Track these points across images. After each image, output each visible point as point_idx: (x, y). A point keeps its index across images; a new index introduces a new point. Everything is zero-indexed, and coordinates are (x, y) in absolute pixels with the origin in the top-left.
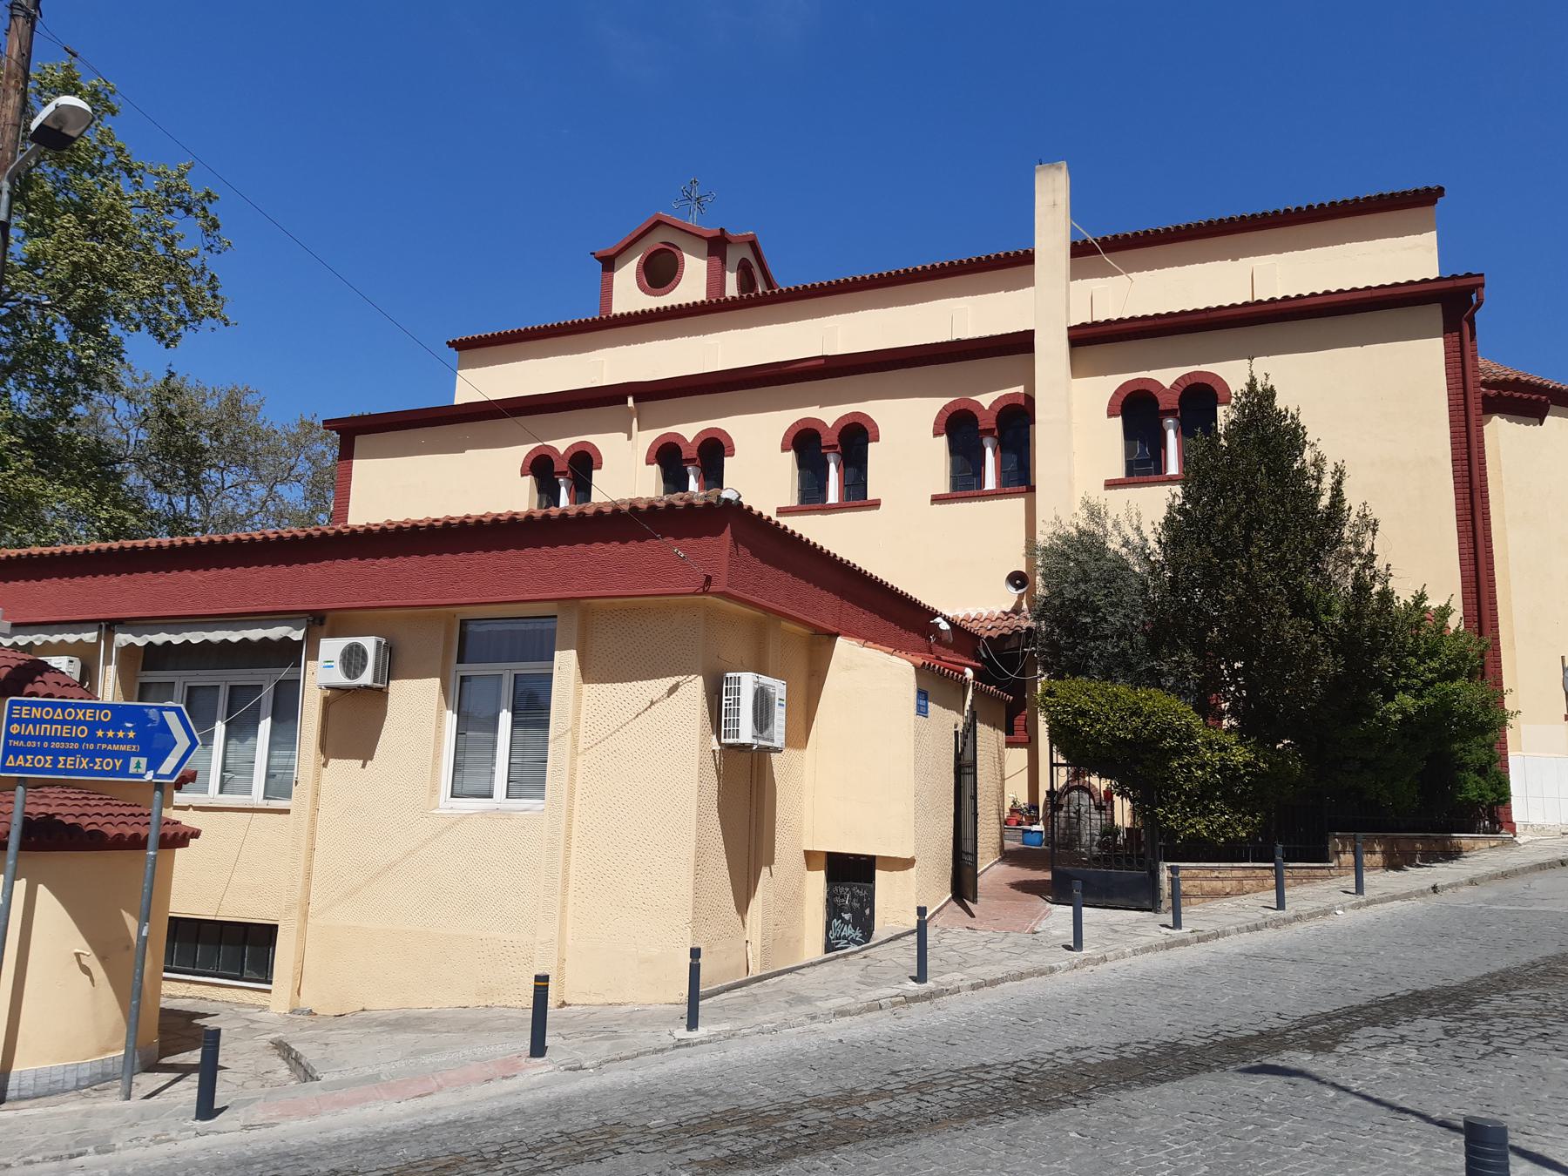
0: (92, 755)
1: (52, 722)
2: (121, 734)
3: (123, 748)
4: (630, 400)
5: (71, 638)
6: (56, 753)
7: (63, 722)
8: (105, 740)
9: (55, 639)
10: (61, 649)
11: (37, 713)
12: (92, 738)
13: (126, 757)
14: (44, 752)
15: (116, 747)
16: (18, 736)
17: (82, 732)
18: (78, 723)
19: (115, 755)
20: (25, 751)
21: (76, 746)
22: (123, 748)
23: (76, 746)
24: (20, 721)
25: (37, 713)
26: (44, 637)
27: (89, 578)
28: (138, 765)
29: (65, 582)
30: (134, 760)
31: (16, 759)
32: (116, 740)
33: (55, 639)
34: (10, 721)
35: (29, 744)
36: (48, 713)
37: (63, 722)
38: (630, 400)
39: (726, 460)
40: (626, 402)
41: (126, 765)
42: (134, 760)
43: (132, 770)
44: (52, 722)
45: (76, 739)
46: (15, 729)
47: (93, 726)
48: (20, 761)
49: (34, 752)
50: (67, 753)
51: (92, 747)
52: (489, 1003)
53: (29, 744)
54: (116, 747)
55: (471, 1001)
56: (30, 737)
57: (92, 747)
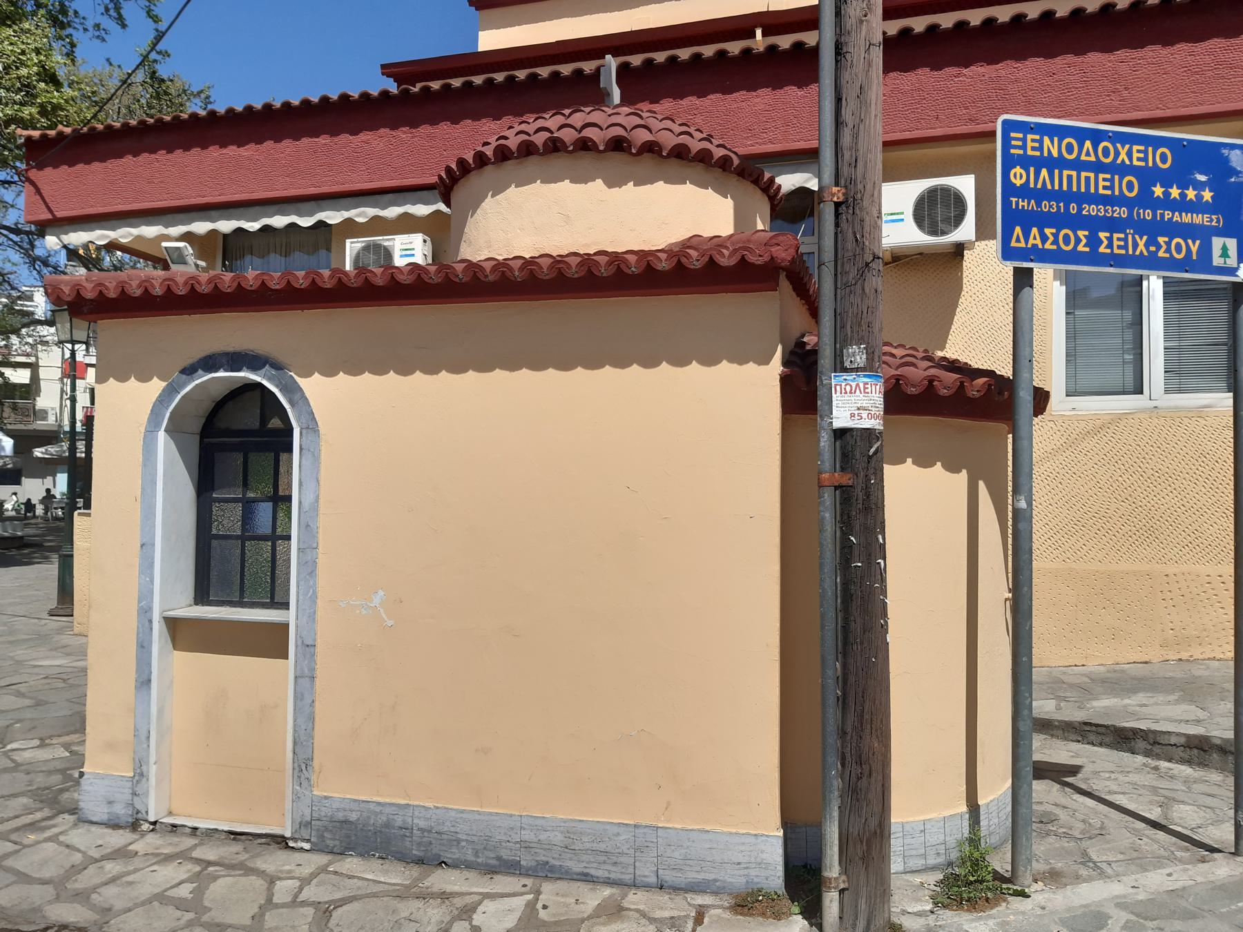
0: (1152, 230)
1: (1078, 165)
2: (1191, 194)
3: (1198, 219)
4: (759, 32)
5: (422, 210)
6: (1094, 225)
7: (1098, 167)
8: (1167, 202)
9: (392, 212)
10: (406, 225)
11: (1051, 147)
12: (1144, 198)
13: (1204, 234)
14: (1077, 222)
15: (1187, 218)
16: (1024, 192)
17: (1128, 187)
18: (1123, 170)
19: (1188, 231)
20: (1042, 220)
21: (1123, 212)
22: (1198, 219)
23: (1123, 212)
24: (1025, 162)
25: (1051, 147)
26: (372, 212)
27: (445, 126)
28: (1225, 254)
29: (403, 134)
30: (1217, 243)
31: (1027, 236)
32: (1183, 205)
33: (392, 212)
34: (1009, 163)
35: (1045, 206)
36: (1070, 149)
37: (1098, 167)
38: (759, 32)
39: (599, 182)
40: (754, 37)
41: (1206, 250)
42: (1217, 243)
43: (1217, 261)
44: (1078, 165)
45: (1121, 201)
46: (1018, 176)
47: (1147, 176)
48: (1035, 239)
49: (1059, 221)
50: (1113, 225)
51: (1148, 215)
52: (1184, 656)
53: (1045, 206)
54: (1187, 218)
55: (1155, 655)
56: (1041, 194)
57: (1148, 215)
